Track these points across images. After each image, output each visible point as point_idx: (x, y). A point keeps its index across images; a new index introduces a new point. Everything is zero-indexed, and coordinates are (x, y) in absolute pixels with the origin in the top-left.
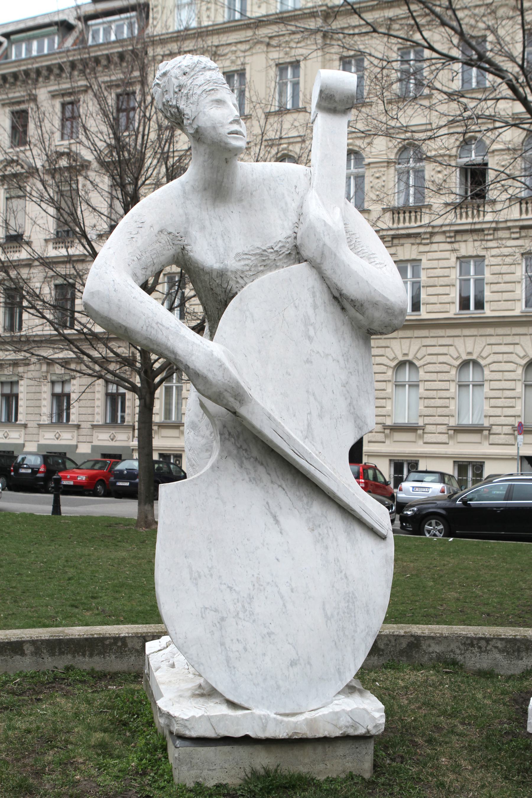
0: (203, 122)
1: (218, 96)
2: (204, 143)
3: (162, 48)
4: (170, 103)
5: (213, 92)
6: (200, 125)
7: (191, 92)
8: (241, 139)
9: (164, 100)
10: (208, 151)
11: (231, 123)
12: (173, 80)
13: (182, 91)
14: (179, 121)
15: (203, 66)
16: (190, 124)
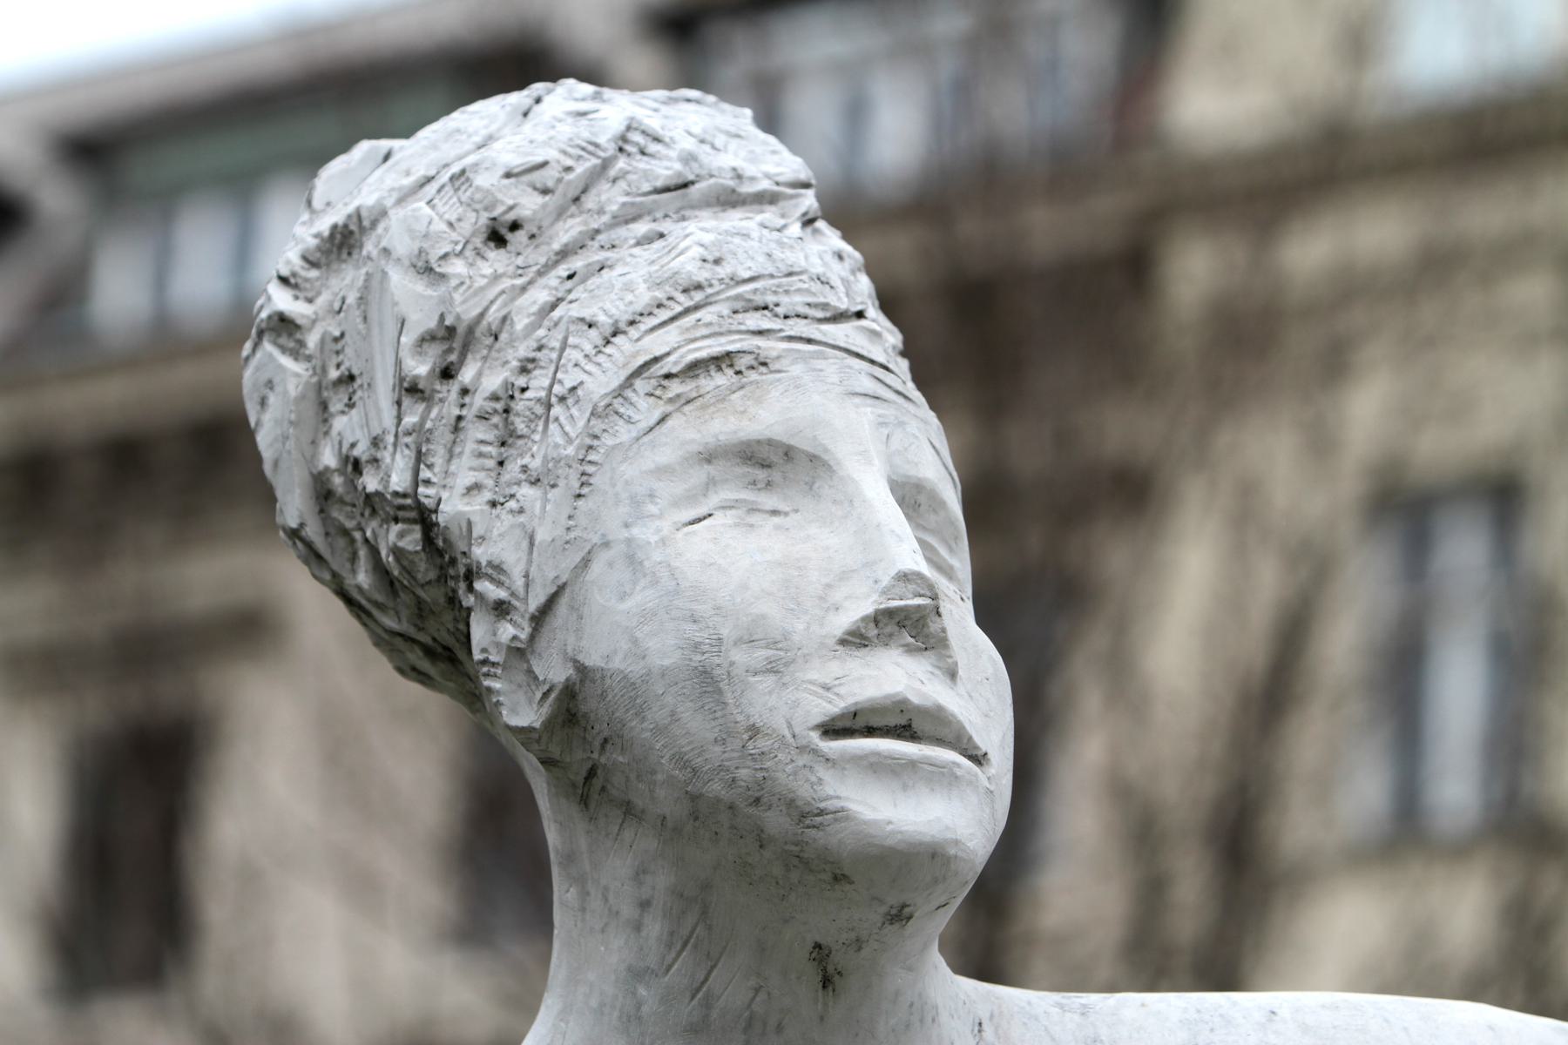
0: (620, 630)
1: (765, 413)
2: (629, 810)
3: (894, 347)
4: (370, 482)
5: (721, 379)
6: (592, 659)
7: (539, 382)
8: (943, 777)
9: (328, 458)
10: (661, 881)
11: (856, 639)
12: (403, 285)
13: (467, 375)
14: (439, 629)
15: (665, 169)
16: (518, 653)
